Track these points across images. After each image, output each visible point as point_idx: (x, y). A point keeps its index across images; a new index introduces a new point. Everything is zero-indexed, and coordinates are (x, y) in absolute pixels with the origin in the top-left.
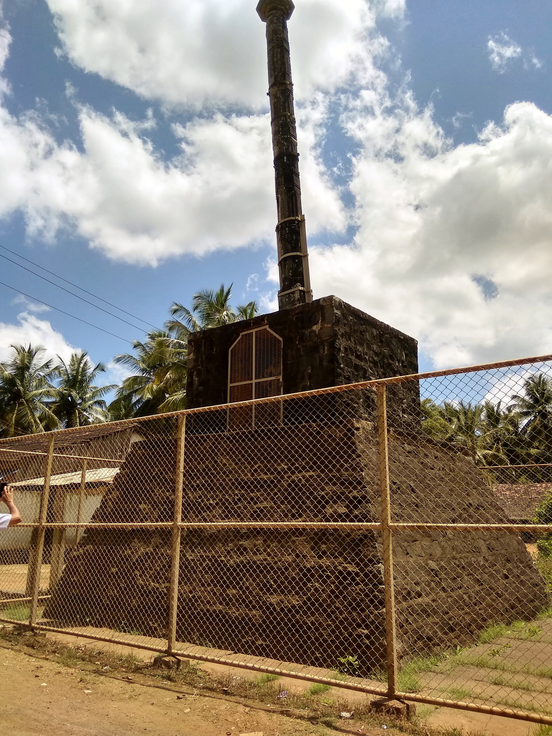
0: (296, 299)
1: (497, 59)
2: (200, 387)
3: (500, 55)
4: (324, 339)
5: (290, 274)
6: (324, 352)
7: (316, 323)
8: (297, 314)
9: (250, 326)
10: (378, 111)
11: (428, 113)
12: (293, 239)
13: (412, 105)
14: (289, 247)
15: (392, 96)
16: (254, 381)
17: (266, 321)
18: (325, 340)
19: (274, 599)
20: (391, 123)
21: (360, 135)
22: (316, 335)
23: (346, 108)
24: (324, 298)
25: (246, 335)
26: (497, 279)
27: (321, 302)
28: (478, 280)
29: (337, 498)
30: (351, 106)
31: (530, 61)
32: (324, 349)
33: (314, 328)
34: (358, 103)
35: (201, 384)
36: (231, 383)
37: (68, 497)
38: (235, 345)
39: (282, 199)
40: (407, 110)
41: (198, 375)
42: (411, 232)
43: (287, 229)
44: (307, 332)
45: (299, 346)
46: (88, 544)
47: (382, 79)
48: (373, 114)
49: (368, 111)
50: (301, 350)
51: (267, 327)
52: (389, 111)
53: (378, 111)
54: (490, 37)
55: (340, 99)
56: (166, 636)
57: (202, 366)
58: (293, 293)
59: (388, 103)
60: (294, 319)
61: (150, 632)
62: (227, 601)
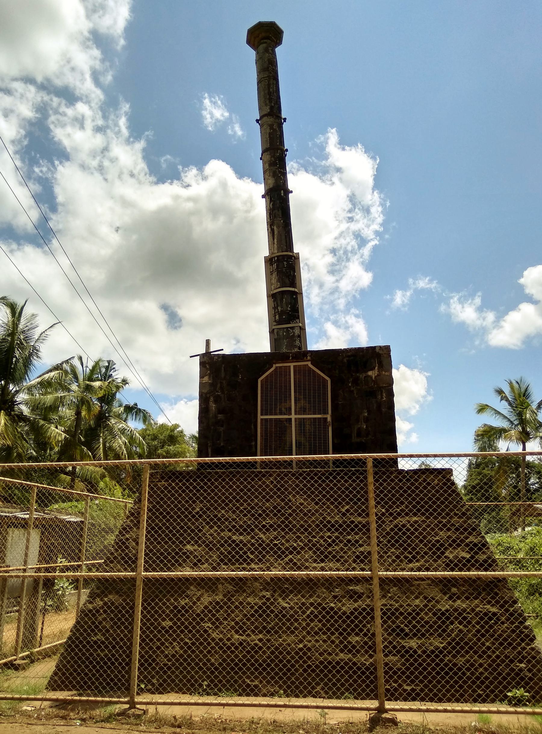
0: (296, 334)
1: (208, 116)
2: (219, 415)
3: (211, 114)
4: (381, 385)
5: (289, 309)
6: (382, 398)
7: (373, 369)
8: (349, 356)
9: (289, 359)
10: (89, 125)
11: (140, 145)
12: (290, 274)
13: (125, 132)
14: (287, 281)
15: (105, 117)
16: (293, 416)
17: (309, 358)
18: (383, 387)
19: (413, 643)
20: (99, 141)
21: (66, 142)
22: (373, 381)
23: (56, 112)
24: (380, 347)
25: (280, 367)
26: (182, 312)
27: (377, 350)
28: (165, 308)
29: (455, 544)
30: (61, 110)
31: (233, 128)
32: (382, 395)
33: (370, 373)
34: (70, 112)
35: (220, 411)
36: (262, 415)
37: (11, 533)
38: (267, 376)
39: (279, 232)
40: (118, 133)
41: (215, 402)
42: (105, 252)
43: (285, 263)
44: (362, 376)
45: (352, 389)
46: (110, 593)
47: (98, 95)
48: (82, 127)
49: (80, 122)
50: (355, 392)
51: (309, 363)
52: (98, 129)
53: (89, 125)
54: (206, 95)
55: (51, 100)
56: (376, 697)
57: (223, 392)
58: (292, 328)
59: (100, 122)
60: (345, 360)
61: (367, 697)
62: (351, 649)
